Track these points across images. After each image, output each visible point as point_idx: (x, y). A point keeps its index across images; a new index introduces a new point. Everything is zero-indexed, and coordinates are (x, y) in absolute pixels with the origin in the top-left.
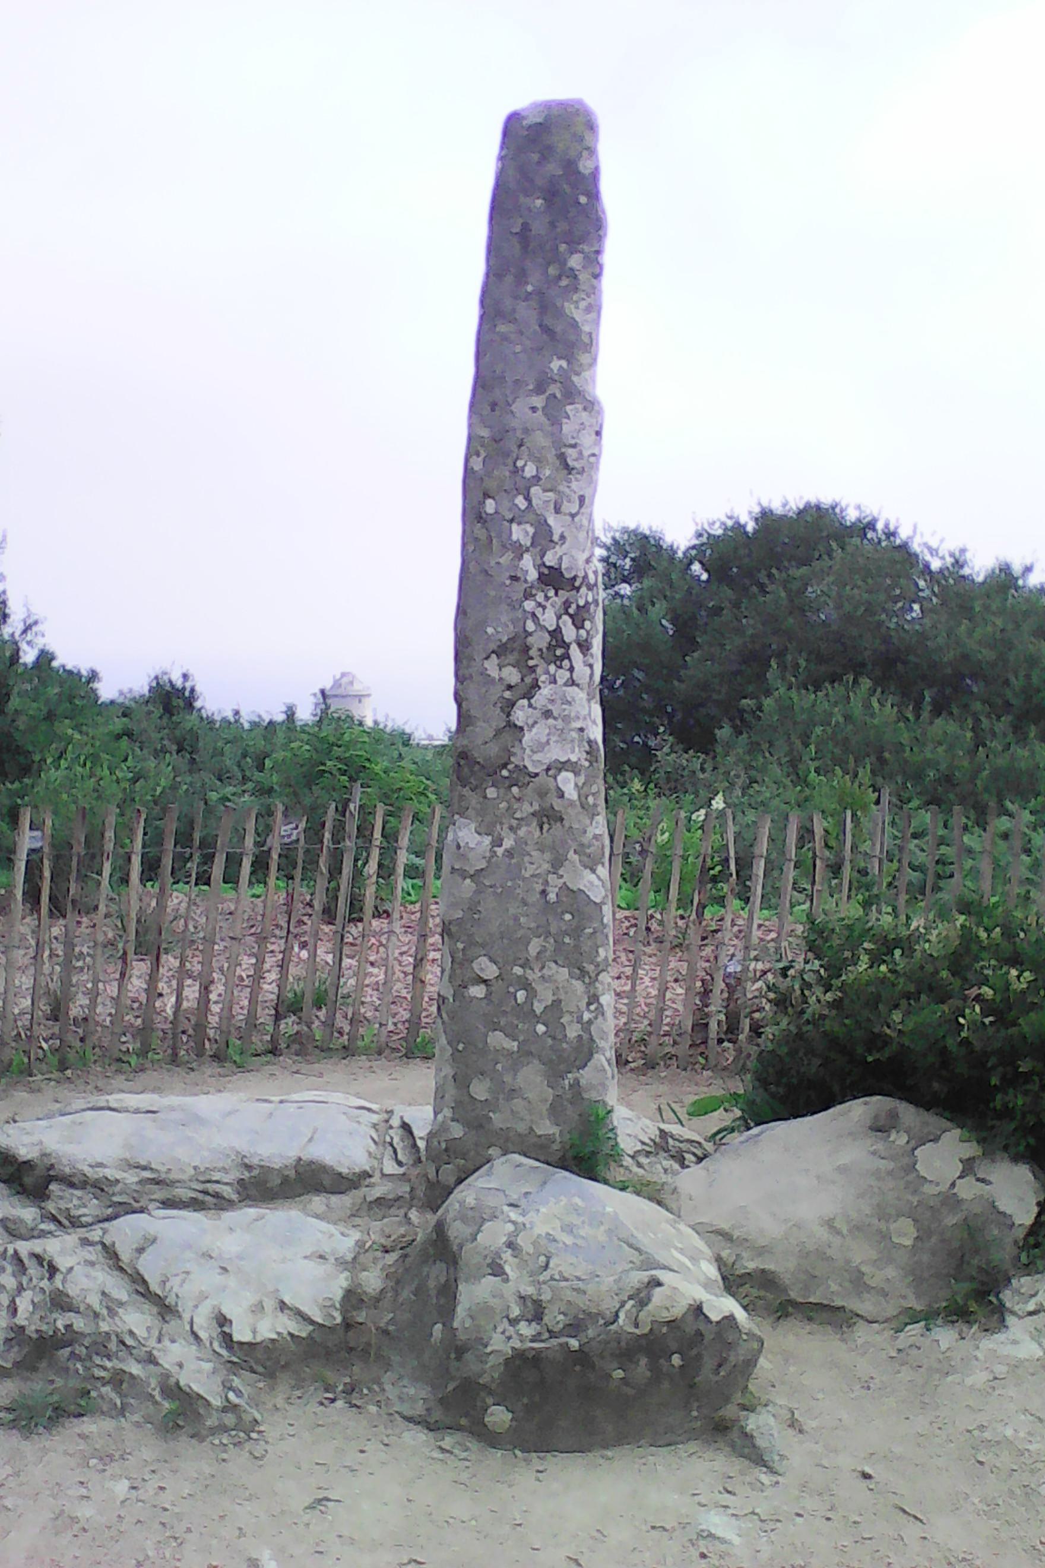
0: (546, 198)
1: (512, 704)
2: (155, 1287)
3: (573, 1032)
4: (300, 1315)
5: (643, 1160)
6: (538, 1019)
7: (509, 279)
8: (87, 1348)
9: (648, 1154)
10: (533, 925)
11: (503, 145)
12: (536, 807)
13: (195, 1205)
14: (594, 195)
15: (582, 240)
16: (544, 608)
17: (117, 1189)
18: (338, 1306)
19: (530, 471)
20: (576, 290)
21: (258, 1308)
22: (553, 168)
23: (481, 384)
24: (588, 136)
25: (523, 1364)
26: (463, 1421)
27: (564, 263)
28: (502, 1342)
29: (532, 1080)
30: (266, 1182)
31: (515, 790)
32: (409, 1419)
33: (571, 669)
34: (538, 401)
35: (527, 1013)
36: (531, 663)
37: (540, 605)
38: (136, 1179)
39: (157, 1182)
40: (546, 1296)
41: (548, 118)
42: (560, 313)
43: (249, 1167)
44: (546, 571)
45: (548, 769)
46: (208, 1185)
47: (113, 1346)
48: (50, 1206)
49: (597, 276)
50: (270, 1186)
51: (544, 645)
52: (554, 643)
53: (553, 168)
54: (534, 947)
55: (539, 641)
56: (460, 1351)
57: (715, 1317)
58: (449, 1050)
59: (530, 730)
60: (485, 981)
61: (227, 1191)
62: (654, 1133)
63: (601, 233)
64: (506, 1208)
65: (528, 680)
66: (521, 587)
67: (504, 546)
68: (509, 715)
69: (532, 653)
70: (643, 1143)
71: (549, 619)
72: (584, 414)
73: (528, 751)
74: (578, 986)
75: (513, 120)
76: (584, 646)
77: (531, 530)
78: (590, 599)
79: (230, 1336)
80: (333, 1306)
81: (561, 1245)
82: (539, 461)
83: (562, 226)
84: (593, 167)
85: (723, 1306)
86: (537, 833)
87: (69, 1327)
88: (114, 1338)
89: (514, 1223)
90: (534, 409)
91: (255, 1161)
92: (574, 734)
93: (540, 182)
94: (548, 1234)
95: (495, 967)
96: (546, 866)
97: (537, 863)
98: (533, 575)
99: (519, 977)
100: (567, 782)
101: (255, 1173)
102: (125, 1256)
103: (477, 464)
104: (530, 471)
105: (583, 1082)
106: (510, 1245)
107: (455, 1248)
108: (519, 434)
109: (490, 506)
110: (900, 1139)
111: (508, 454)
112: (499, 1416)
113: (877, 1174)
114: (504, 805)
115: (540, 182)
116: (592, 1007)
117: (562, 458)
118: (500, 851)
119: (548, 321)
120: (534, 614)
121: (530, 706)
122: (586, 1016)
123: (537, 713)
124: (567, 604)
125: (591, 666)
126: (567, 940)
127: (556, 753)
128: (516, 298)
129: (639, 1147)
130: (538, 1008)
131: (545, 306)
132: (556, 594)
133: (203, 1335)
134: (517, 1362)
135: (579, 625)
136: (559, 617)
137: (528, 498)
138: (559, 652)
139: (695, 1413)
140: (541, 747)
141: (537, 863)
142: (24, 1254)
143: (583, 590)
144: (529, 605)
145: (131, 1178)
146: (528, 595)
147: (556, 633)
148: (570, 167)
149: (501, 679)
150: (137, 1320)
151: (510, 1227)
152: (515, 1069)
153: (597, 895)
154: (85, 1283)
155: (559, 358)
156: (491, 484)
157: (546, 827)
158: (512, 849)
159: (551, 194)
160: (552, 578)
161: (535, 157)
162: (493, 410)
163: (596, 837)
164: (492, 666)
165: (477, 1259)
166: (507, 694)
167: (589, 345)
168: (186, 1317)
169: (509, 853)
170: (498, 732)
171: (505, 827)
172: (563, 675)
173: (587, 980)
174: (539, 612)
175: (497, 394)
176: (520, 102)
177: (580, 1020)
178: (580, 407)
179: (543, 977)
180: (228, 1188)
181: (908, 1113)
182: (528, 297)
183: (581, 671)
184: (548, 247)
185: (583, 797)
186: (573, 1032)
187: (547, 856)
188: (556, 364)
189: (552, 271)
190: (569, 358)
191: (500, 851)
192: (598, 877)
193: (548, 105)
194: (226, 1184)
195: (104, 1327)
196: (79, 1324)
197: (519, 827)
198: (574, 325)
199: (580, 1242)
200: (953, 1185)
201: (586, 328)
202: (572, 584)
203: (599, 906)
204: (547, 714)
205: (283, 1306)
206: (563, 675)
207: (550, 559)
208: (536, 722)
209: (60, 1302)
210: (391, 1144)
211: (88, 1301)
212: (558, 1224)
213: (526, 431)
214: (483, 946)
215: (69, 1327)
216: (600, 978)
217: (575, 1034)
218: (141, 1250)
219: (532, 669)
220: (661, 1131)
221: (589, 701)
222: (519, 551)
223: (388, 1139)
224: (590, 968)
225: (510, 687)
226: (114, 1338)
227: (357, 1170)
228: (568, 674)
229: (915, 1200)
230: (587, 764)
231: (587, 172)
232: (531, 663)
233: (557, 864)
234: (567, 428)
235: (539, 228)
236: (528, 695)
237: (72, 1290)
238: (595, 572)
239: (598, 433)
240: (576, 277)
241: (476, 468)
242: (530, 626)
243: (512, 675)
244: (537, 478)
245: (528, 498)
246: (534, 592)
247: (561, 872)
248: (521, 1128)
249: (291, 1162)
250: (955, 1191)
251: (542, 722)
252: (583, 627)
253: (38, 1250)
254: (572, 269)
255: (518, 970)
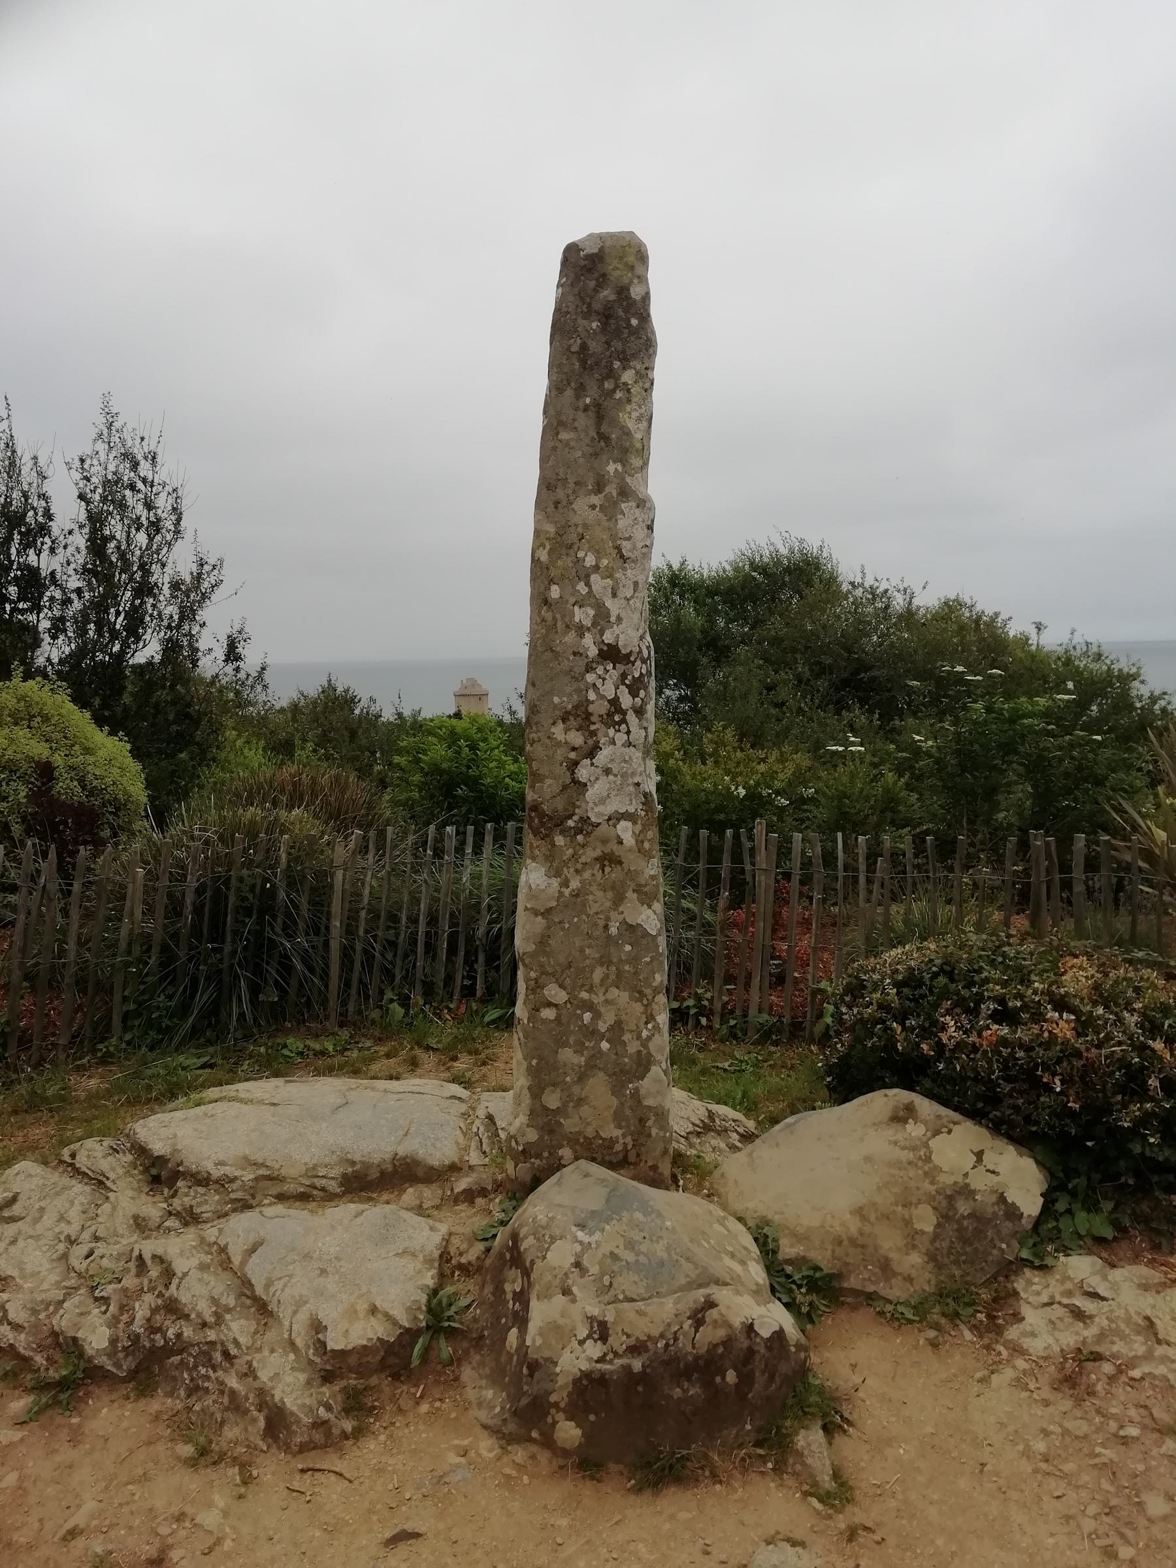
0: (602, 314)
1: (576, 763)
2: (259, 1291)
3: (633, 1047)
4: (388, 1317)
5: (696, 1141)
6: (602, 1037)
7: (569, 393)
8: (194, 1357)
9: (698, 1134)
10: (597, 956)
11: (562, 273)
12: (598, 853)
13: (304, 1197)
14: (645, 318)
15: (634, 356)
16: (604, 679)
17: (235, 1186)
18: (424, 1308)
19: (590, 560)
20: (629, 401)
21: (352, 1314)
22: (607, 294)
23: (547, 484)
24: (639, 270)
25: (590, 1390)
26: (535, 1434)
27: (617, 378)
28: (576, 1359)
29: (598, 1088)
30: (366, 1175)
31: (580, 838)
32: (485, 1427)
33: (628, 733)
34: (596, 500)
35: (592, 1033)
36: (593, 727)
37: (600, 677)
38: (252, 1176)
39: (269, 1178)
40: (610, 1318)
41: (601, 249)
42: (615, 422)
43: (353, 1163)
44: (605, 648)
45: (609, 819)
46: (315, 1180)
47: (218, 1357)
48: (177, 1203)
49: (648, 390)
50: (366, 1182)
51: (603, 711)
52: (613, 709)
53: (607, 294)
54: (598, 974)
55: (599, 708)
56: (534, 1366)
57: (765, 1333)
58: (525, 1064)
59: (592, 786)
60: (556, 1006)
61: (333, 1186)
62: (702, 1113)
63: (651, 351)
64: (574, 1229)
65: (591, 742)
66: (581, 664)
67: (567, 626)
68: (573, 773)
69: (592, 719)
70: (694, 1124)
71: (609, 691)
72: (637, 511)
73: (591, 805)
74: (638, 1007)
75: (571, 251)
76: (640, 712)
77: (592, 612)
78: (644, 671)
79: (324, 1344)
80: (419, 1308)
81: (624, 1263)
82: (599, 554)
83: (617, 345)
84: (643, 293)
85: (774, 1317)
86: (599, 875)
87: (179, 1336)
88: (219, 1347)
89: (581, 1243)
90: (593, 507)
91: (357, 1158)
92: (632, 788)
93: (597, 306)
94: (612, 1253)
95: (564, 993)
96: (608, 904)
97: (599, 900)
98: (593, 652)
99: (585, 1001)
100: (625, 830)
101: (358, 1167)
102: (236, 1260)
103: (543, 556)
104: (590, 560)
105: (642, 1092)
106: (577, 1265)
107: (528, 1264)
108: (580, 529)
109: (555, 592)
110: (915, 1130)
111: (570, 547)
112: (569, 1432)
113: (898, 1164)
114: (571, 851)
115: (597, 306)
116: (650, 1026)
117: (618, 548)
118: (567, 892)
119: (604, 428)
120: (594, 685)
121: (592, 764)
122: (645, 1034)
123: (599, 771)
124: (624, 676)
125: (645, 728)
126: (627, 968)
127: (616, 805)
128: (577, 409)
129: (691, 1128)
130: (602, 1027)
131: (600, 413)
132: (614, 668)
133: (299, 1342)
134: (585, 1382)
135: (634, 693)
136: (617, 688)
137: (588, 584)
138: (617, 718)
139: (748, 1427)
140: (602, 801)
141: (599, 900)
142: (147, 1257)
143: (638, 663)
144: (590, 678)
145: (248, 1176)
146: (589, 669)
147: (615, 702)
148: (623, 291)
149: (566, 743)
150: (239, 1328)
151: (578, 1248)
152: (582, 1078)
153: (677, 1094)
154: (200, 1290)
155: (614, 462)
156: (553, 573)
157: (607, 869)
158: (579, 890)
159: (606, 315)
160: (611, 654)
161: (592, 284)
162: (556, 507)
163: (653, 877)
164: (558, 731)
165: (548, 1277)
166: (573, 755)
167: (643, 451)
168: (287, 1324)
169: (576, 895)
170: (565, 788)
171: (572, 870)
172: (621, 738)
173: (645, 1002)
174: (599, 683)
175: (560, 494)
176: (576, 235)
177: (639, 1037)
178: (633, 504)
179: (607, 1001)
180: (333, 1183)
181: (926, 1107)
182: (586, 409)
183: (637, 734)
184: (603, 363)
185: (640, 842)
186: (633, 1047)
187: (610, 894)
188: (611, 468)
189: (608, 385)
190: (623, 461)
191: (567, 892)
192: (654, 912)
193: (601, 237)
194: (333, 1178)
195: (212, 1335)
196: (188, 1332)
197: (584, 869)
198: (628, 434)
199: (642, 1259)
200: (966, 1175)
201: (638, 436)
202: (626, 659)
203: (654, 937)
204: (607, 771)
205: (373, 1310)
206: (621, 738)
207: (608, 637)
208: (597, 779)
209: (173, 1308)
210: (477, 1134)
211: (198, 1308)
212: (621, 1242)
213: (586, 526)
214: (553, 974)
215: (179, 1336)
216: (656, 999)
217: (634, 1050)
218: (253, 1250)
219: (593, 734)
220: (710, 1111)
221: (644, 759)
222: (581, 630)
223: (475, 1130)
224: (648, 991)
225: (574, 749)
226: (219, 1347)
227: (447, 1162)
228: (626, 737)
229: (932, 1188)
230: (643, 813)
231: (638, 298)
232: (593, 727)
233: (619, 900)
234: (622, 523)
235: (595, 346)
236: (592, 753)
237: (184, 1298)
238: (648, 647)
239: (650, 528)
240: (628, 391)
241: (542, 559)
242: (592, 696)
243: (576, 738)
244: (596, 568)
245: (588, 584)
246: (594, 665)
247: (621, 909)
248: (590, 1132)
249: (388, 1157)
250: (967, 1181)
251: (603, 778)
252: (638, 696)
253: (160, 1251)
254: (625, 384)
255: (584, 995)
